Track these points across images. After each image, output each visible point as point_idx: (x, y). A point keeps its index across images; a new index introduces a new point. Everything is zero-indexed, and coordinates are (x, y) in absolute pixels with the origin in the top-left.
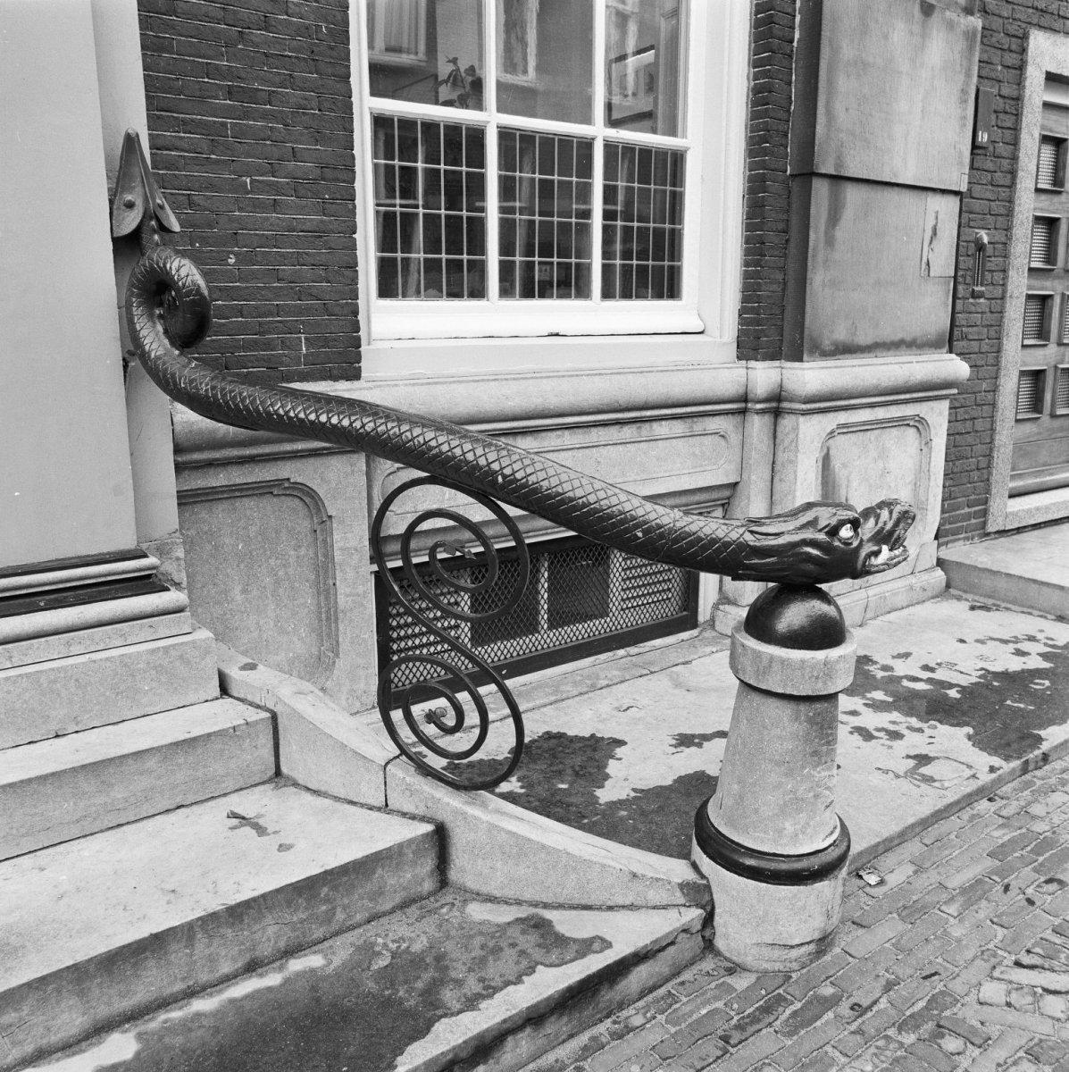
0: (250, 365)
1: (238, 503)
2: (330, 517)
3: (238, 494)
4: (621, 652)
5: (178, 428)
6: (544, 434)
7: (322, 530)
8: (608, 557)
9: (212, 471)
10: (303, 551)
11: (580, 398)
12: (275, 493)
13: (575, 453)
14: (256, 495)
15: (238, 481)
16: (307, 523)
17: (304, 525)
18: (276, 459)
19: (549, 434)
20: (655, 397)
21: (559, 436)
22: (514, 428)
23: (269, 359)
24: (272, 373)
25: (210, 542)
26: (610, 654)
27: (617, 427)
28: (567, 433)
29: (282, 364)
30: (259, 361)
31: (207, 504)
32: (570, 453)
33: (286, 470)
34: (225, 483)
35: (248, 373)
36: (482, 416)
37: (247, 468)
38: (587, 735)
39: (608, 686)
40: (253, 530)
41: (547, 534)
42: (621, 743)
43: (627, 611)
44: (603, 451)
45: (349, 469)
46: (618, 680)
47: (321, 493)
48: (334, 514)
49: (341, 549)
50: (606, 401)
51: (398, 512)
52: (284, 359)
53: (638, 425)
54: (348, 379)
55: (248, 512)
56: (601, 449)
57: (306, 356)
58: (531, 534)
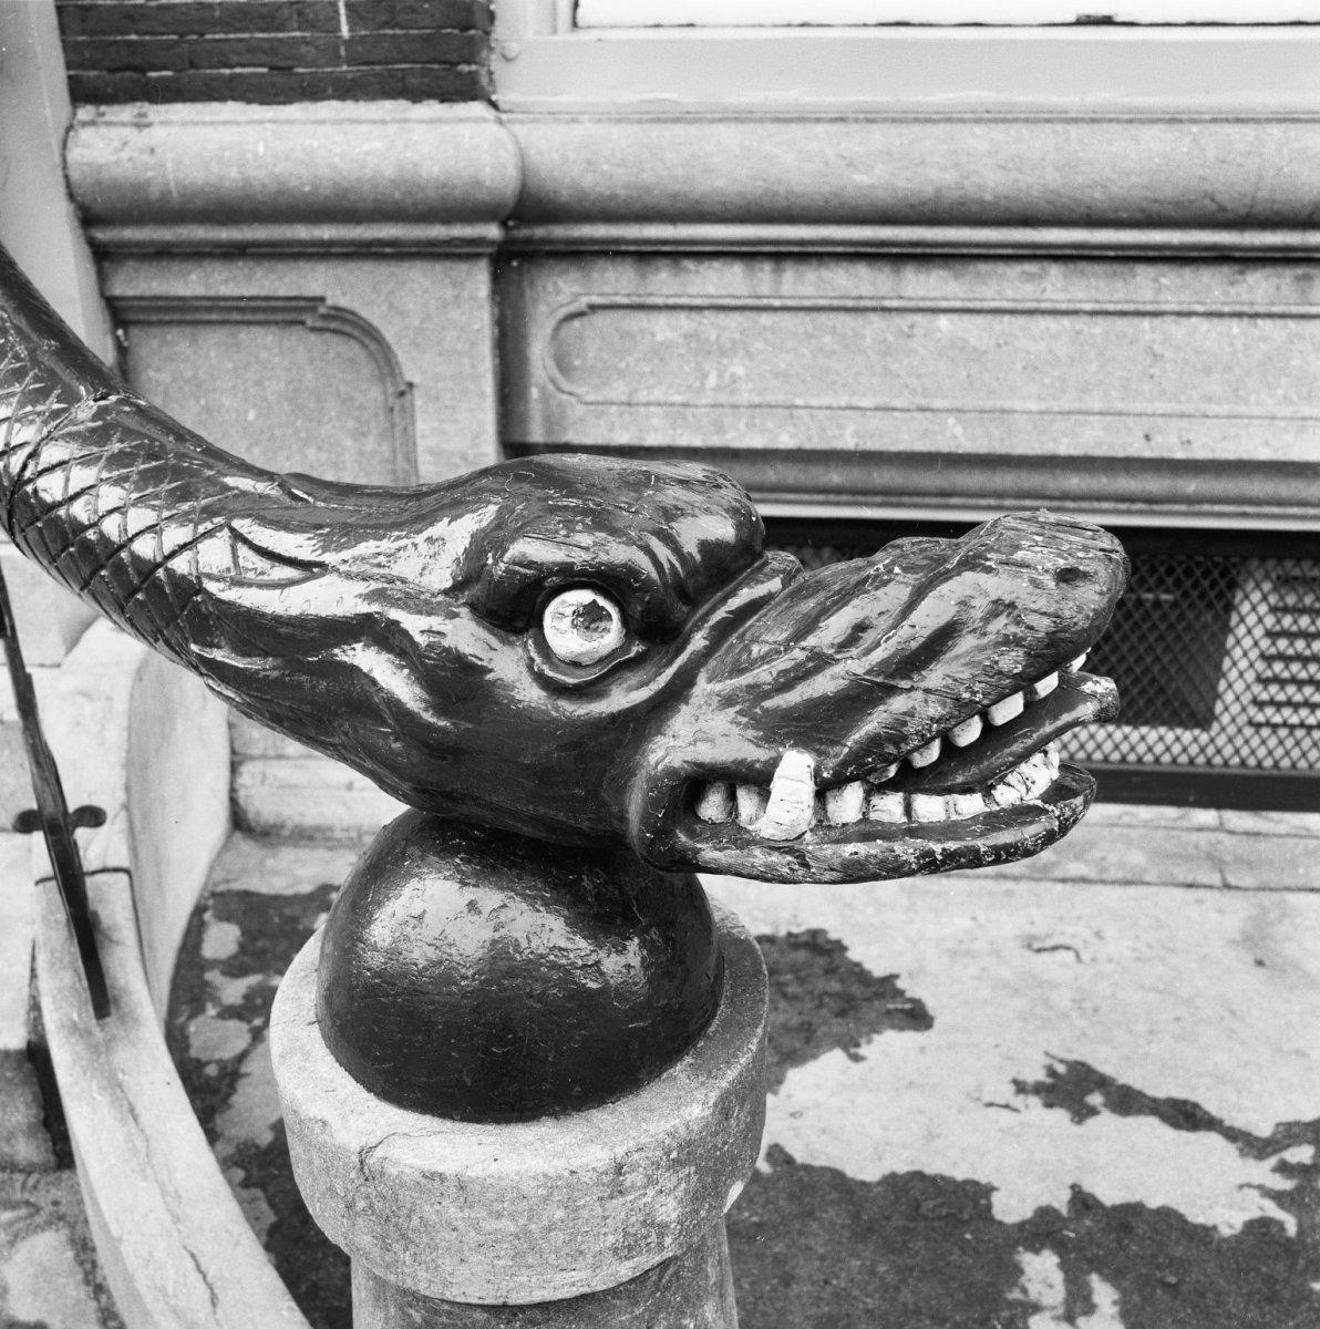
0: (235, 59)
1: (244, 334)
2: (411, 385)
3: (236, 316)
4: (1206, 816)
5: (75, 175)
6: (983, 267)
7: (403, 410)
8: (1229, 607)
9: (176, 266)
10: (370, 444)
11: (1080, 179)
12: (309, 323)
13: (1080, 323)
14: (276, 323)
15: (225, 290)
16: (375, 392)
17: (372, 395)
18: (297, 256)
19: (1001, 268)
20: (603, 189)
21: (1030, 277)
22: (883, 243)
23: (273, 48)
24: (279, 79)
25: (197, 399)
26: (1170, 812)
27: (1227, 270)
28: (1055, 271)
29: (301, 61)
30: (252, 53)
31: (188, 330)
32: (1066, 321)
33: (315, 280)
34: (201, 291)
35: (233, 76)
36: (975, 208)
37: (241, 267)
38: (878, 969)
39: (1084, 880)
40: (273, 388)
41: (1245, 515)
42: (917, 1017)
43: (1300, 733)
44: (1178, 329)
45: (449, 293)
46: (1120, 875)
47: (389, 333)
48: (416, 380)
49: (431, 452)
50: (1168, 192)
51: (590, 398)
52: (304, 49)
53: (1300, 271)
54: (445, 98)
55: (264, 355)
56: (1169, 324)
57: (348, 43)
58: (953, 501)
